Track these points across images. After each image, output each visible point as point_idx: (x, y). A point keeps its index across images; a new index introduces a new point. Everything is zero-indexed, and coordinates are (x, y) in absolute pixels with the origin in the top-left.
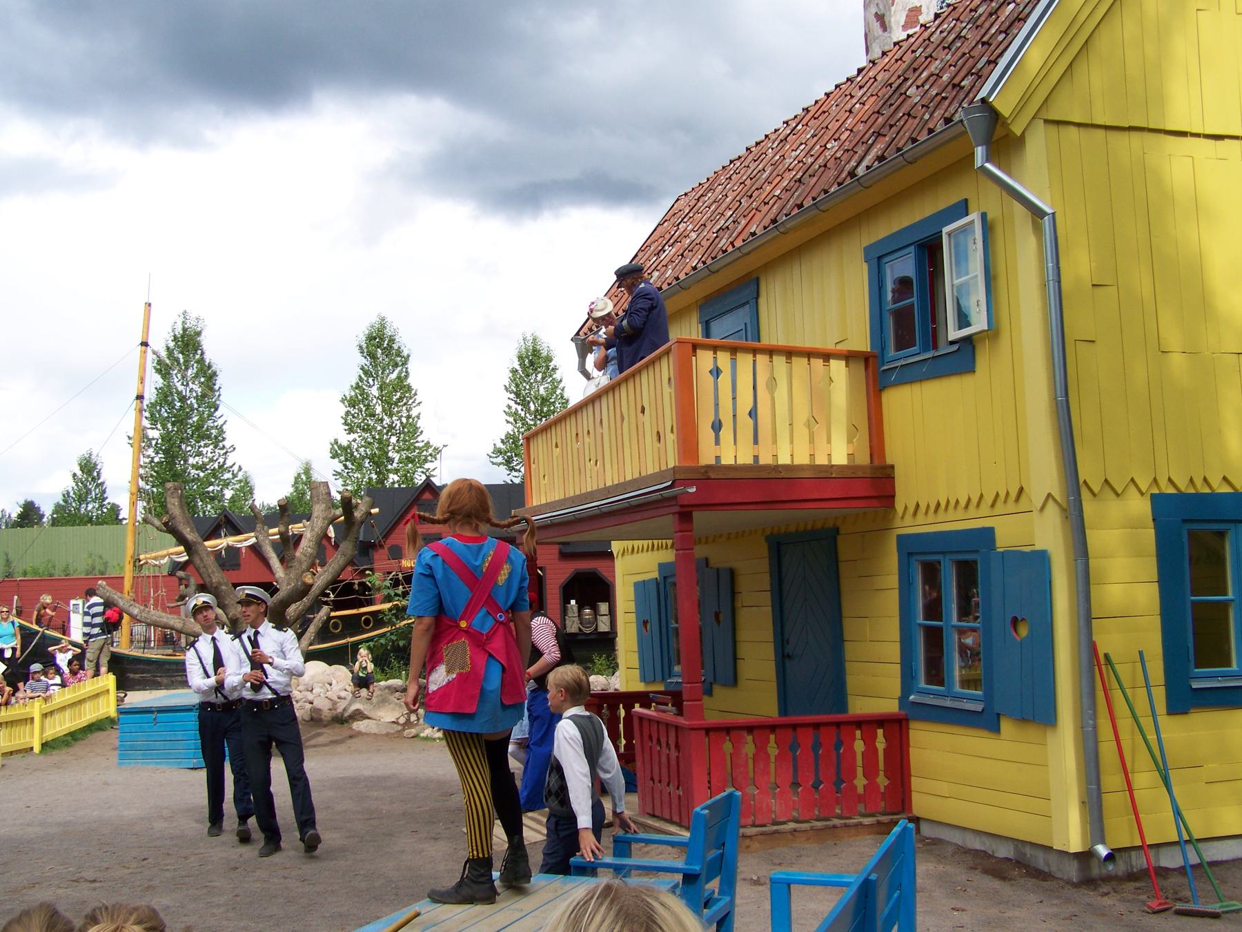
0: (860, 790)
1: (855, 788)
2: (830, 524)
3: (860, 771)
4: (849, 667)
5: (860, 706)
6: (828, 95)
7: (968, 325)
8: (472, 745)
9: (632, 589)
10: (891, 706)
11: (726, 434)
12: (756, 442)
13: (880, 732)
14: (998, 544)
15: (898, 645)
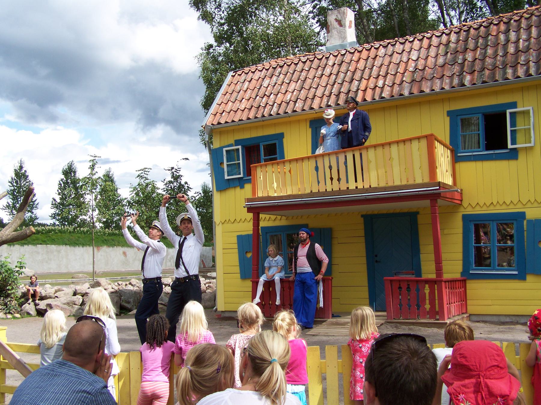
0: (428, 310)
1: (426, 309)
2: (415, 210)
3: (427, 302)
4: (422, 263)
5: (425, 276)
6: (226, 122)
7: (515, 144)
8: (455, 297)
9: (236, 238)
10: (458, 276)
11: (335, 181)
12: (356, 181)
13: (427, 286)
14: (526, 218)
15: (434, 254)
